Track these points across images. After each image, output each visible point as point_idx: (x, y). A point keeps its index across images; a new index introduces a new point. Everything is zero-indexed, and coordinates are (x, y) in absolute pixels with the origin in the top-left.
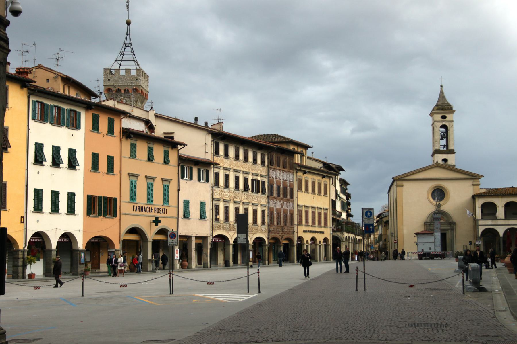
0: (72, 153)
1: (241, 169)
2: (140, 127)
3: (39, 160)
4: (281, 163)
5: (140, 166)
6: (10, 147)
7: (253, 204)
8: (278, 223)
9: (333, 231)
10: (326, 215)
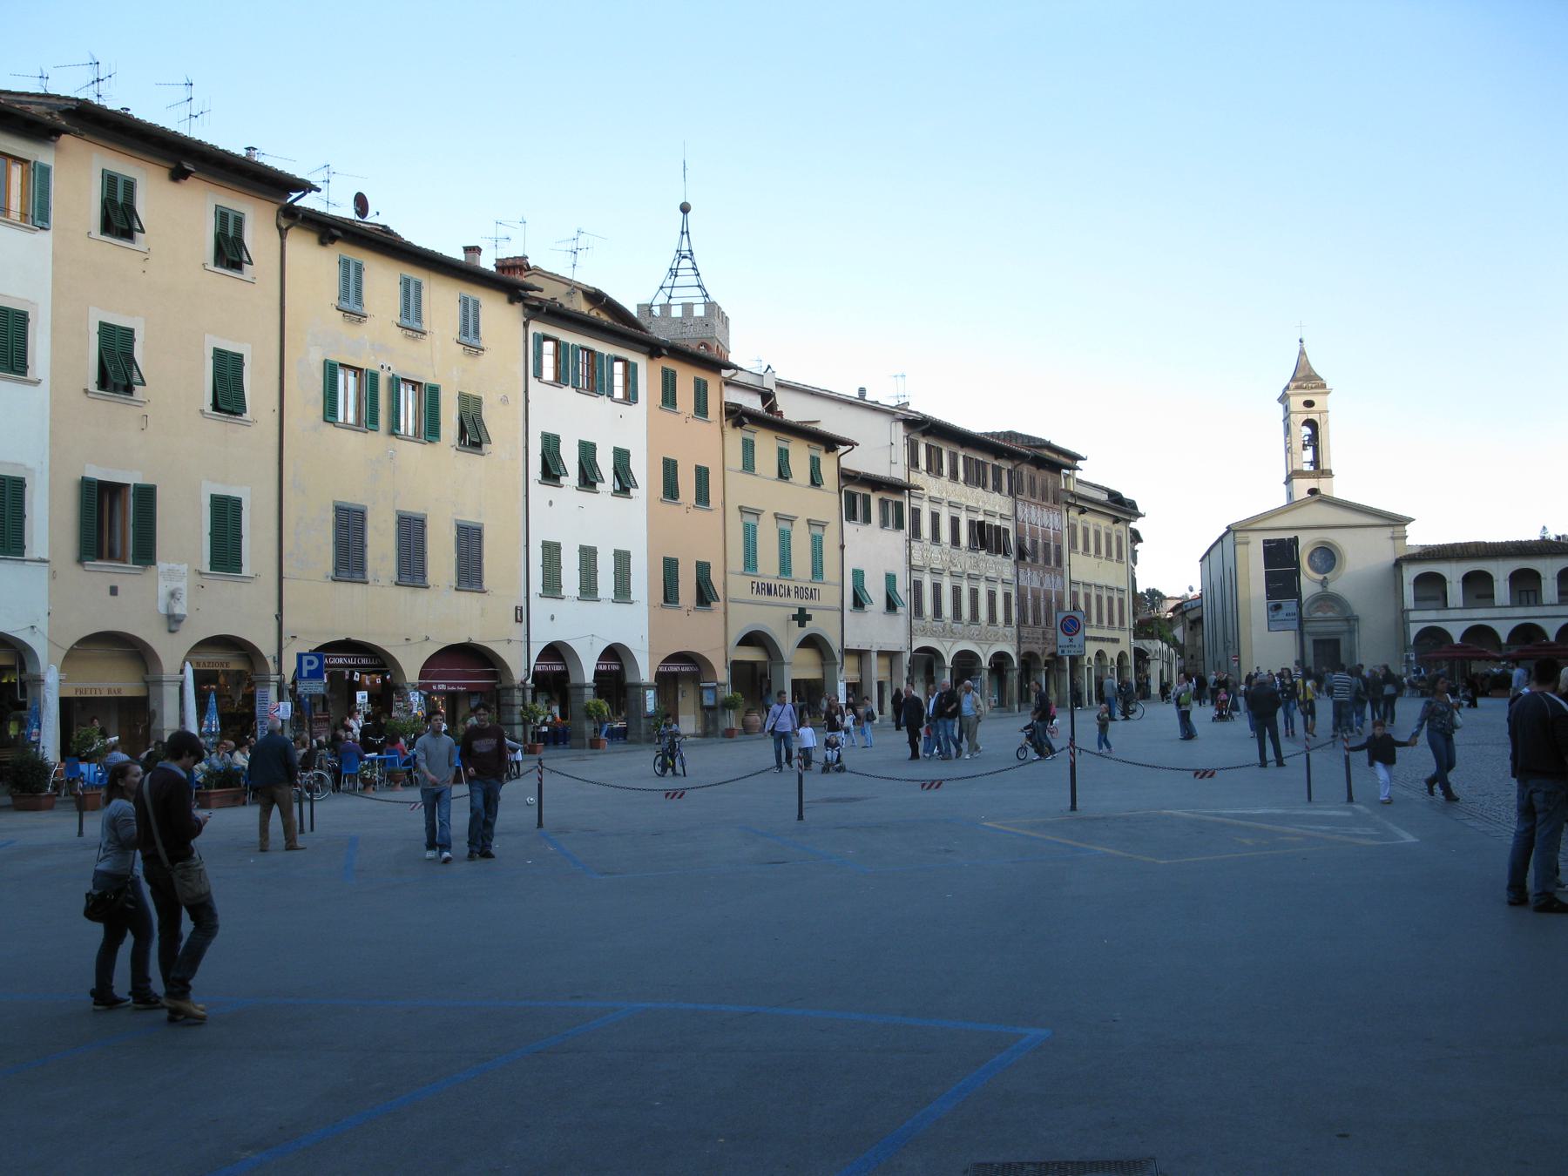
0: (622, 457)
1: (963, 500)
2: (754, 403)
3: (551, 473)
4: (1038, 491)
5: (761, 490)
6: (489, 442)
7: (987, 579)
8: (1036, 621)
9: (1136, 637)
10: (1121, 601)
